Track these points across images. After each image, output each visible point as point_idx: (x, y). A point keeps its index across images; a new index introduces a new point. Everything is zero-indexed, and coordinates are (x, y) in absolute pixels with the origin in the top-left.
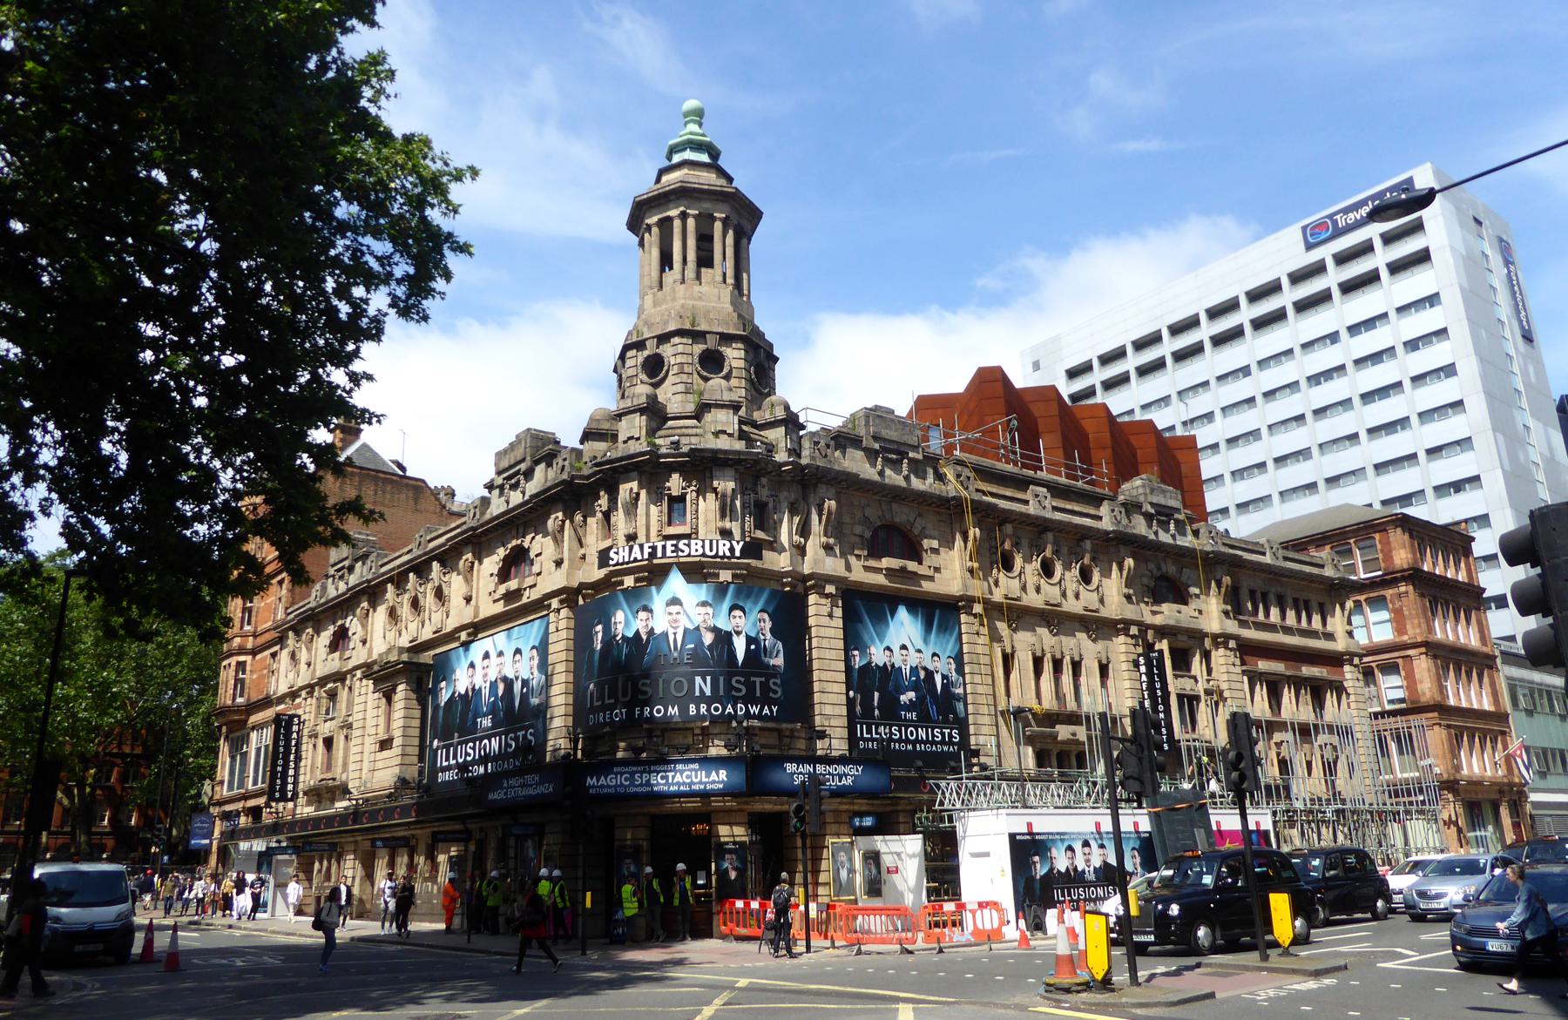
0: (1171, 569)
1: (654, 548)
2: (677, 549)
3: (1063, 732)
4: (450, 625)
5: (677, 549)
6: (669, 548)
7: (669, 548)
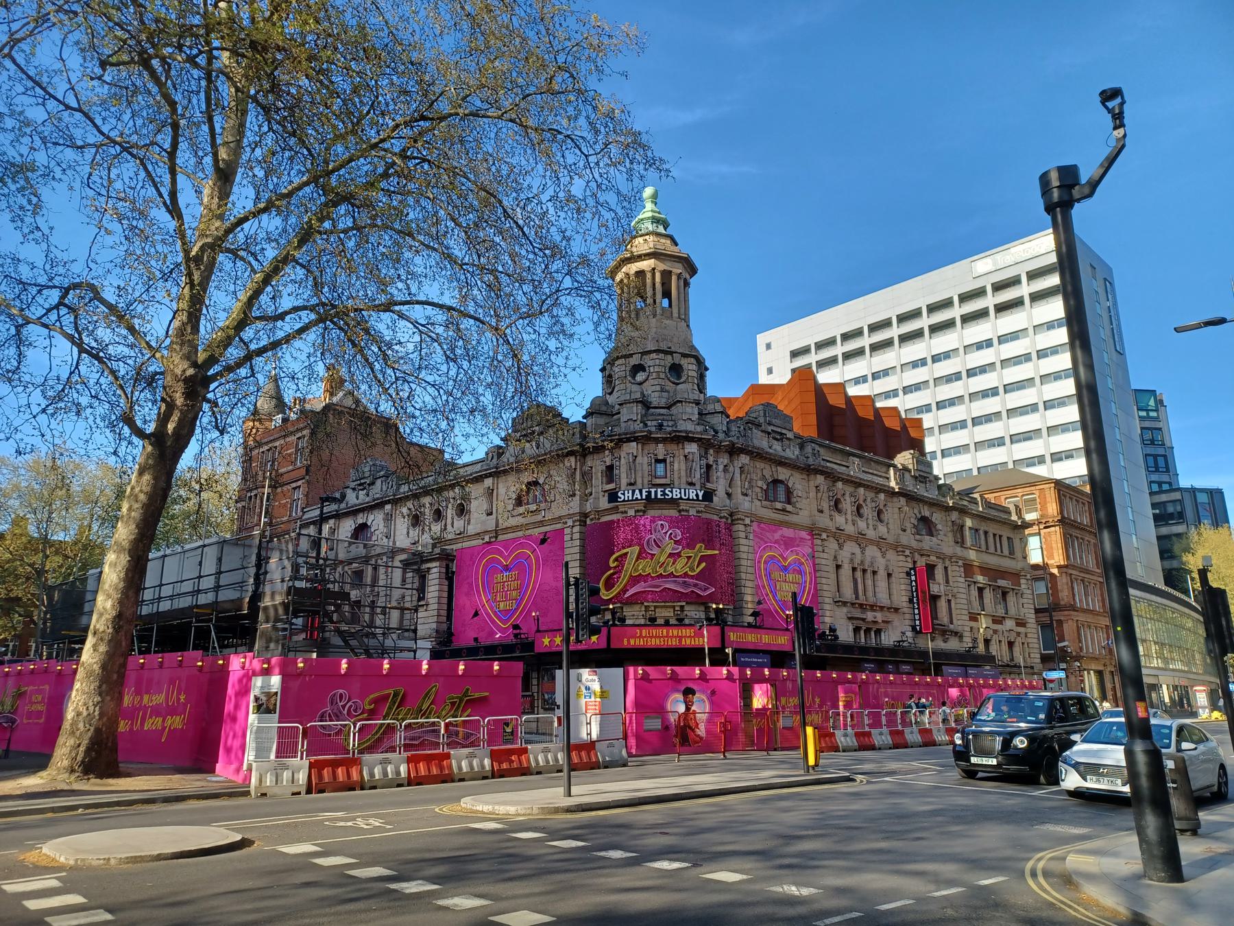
0: (926, 512)
1: (649, 492)
2: (664, 494)
3: (870, 616)
4: (471, 529)
5: (664, 494)
6: (659, 493)
7: (659, 493)
